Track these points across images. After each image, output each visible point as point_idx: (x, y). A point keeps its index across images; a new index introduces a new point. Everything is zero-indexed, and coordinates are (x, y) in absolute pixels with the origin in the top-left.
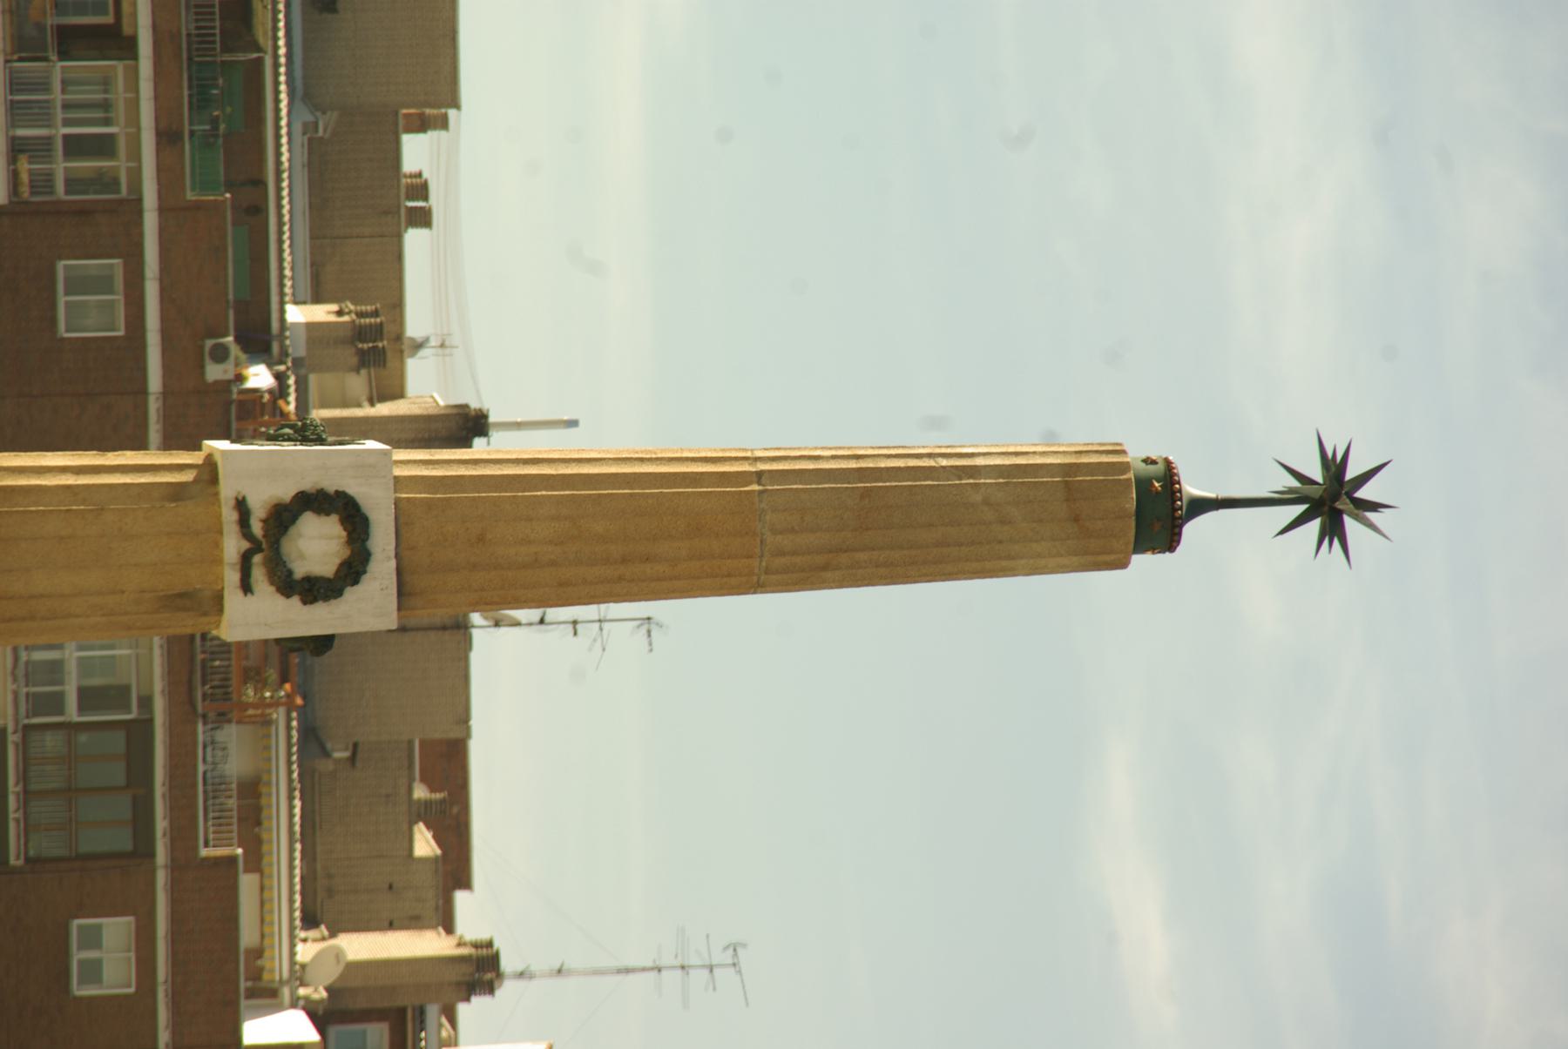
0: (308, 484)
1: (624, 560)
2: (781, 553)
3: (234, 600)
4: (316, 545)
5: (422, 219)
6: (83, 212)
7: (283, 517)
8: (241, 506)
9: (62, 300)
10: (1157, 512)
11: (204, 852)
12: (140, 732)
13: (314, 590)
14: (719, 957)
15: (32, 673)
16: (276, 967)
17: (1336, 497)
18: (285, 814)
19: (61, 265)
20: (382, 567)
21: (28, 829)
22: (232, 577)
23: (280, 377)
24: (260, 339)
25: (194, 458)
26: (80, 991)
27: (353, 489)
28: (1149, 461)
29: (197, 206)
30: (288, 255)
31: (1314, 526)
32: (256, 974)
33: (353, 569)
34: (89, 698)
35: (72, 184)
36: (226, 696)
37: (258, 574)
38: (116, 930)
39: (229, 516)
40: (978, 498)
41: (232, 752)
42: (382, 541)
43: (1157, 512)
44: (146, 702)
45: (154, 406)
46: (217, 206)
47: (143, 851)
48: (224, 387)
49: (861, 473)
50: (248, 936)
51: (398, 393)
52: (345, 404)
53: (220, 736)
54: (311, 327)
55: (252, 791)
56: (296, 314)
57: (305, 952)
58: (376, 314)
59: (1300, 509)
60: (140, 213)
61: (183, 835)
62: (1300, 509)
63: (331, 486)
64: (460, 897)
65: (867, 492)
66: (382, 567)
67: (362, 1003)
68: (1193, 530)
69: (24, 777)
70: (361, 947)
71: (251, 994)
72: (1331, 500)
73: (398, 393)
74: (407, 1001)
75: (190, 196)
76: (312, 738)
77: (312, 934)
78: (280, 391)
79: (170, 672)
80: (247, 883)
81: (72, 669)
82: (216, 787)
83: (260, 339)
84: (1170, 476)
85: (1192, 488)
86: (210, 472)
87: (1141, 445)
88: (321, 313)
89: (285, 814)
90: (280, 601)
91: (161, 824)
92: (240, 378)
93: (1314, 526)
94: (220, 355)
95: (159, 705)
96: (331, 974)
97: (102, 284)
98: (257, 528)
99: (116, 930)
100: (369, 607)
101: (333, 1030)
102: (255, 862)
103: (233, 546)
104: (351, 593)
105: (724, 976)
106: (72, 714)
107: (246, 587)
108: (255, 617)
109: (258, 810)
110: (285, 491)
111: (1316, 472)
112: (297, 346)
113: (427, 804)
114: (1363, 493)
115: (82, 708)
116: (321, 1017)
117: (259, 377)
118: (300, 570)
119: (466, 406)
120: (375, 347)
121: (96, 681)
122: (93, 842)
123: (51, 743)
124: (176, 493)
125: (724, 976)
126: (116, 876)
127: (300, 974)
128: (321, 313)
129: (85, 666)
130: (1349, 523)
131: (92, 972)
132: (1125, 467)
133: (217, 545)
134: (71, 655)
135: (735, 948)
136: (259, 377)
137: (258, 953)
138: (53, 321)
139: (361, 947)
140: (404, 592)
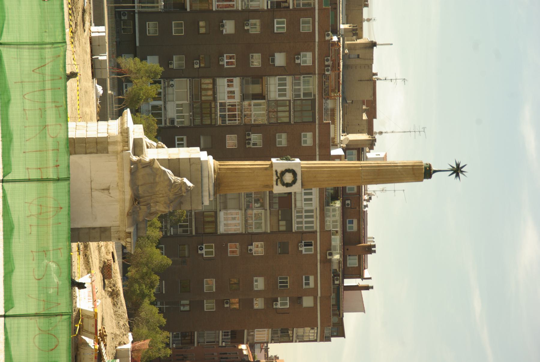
0: (287, 168)
1: (339, 180)
2: (365, 179)
3: (275, 187)
4: (288, 178)
5: (367, 6)
6: (306, 10)
7: (283, 173)
8: (276, 171)
9: (301, 25)
10: (428, 172)
11: (324, 122)
12: (314, 101)
13: (288, 185)
14: (421, 130)
15: (295, 90)
16: (337, 141)
17: (458, 170)
18: (340, 114)
19: (301, 19)
20: (299, 182)
21: (294, 117)
22: (275, 183)
23: (339, 39)
24: (335, 31)
25: (269, 163)
26: (303, 145)
27: (294, 169)
28: (427, 164)
29: (325, 9)
30: (341, 17)
31: (455, 175)
32: (334, 142)
33: (294, 182)
34: (305, 94)
35: (304, 5)
36: (328, 95)
37: (279, 183)
38: (309, 135)
39: (274, 173)
40: (398, 170)
41: (330, 104)
42: (299, 177)
43: (428, 172)
44: (315, 95)
45: (317, 44)
46: (328, 9)
47: (314, 121)
48: (329, 41)
49: (378, 166)
50: (332, 135)
51: (361, 37)
52: (352, 41)
53: (327, 102)
54: (345, 29)
55: (333, 111)
56: (342, 26)
57: (342, 138)
58: (356, 26)
59: (452, 172)
60: (315, 10)
61: (321, 119)
62: (452, 172)
63: (291, 168)
64: (374, 120)
65: (379, 170)
66: (299, 182)
67: (352, 147)
68: (434, 176)
69: (294, 108)
70: (352, 137)
71: (333, 145)
72: (457, 171)
73: (361, 37)
74: (360, 147)
75: (324, 7)
76: (344, 100)
77: (344, 134)
78: (339, 41)
79: (319, 91)
80: (332, 126)
81: (302, 89)
82: (326, 110)
83: (335, 31)
84: (430, 167)
85: (434, 168)
86: (271, 165)
87: (425, 161)
88: (347, 26)
89: (340, 114)
90: (282, 187)
91: (317, 117)
92: (332, 39)
93: (455, 175)
94: (328, 35)
95: (317, 96)
96: (347, 142)
97: (308, 22)
98: (279, 175)
99: (309, 135)
100: (296, 188)
101: (347, 151)
102: (333, 122)
103: (275, 178)
104: (294, 186)
105: (422, 133)
106: (302, 97)
107: (277, 184)
108: (279, 189)
109: (334, 114)
110: (283, 169)
111: (455, 167)
112: (342, 32)
113: (366, 109)
114: (462, 170)
115: (304, 96)
116: (344, 150)
117: (335, 39)
118: (286, 182)
119: (372, 41)
120: (356, 32)
121: (306, 92)
122: (305, 120)
123: (299, 102)
124: (266, 169)
125: (422, 133)
126: (309, 125)
127: (341, 142)
128: (347, 26)
129: (304, 89)
130: (460, 174)
131: (305, 142)
132: (422, 165)
133: (273, 178)
134: (302, 87)
135: (424, 128)
136: (335, 39)
137: (334, 138)
138: (300, 29)
139: (352, 137)
140: (303, 185)
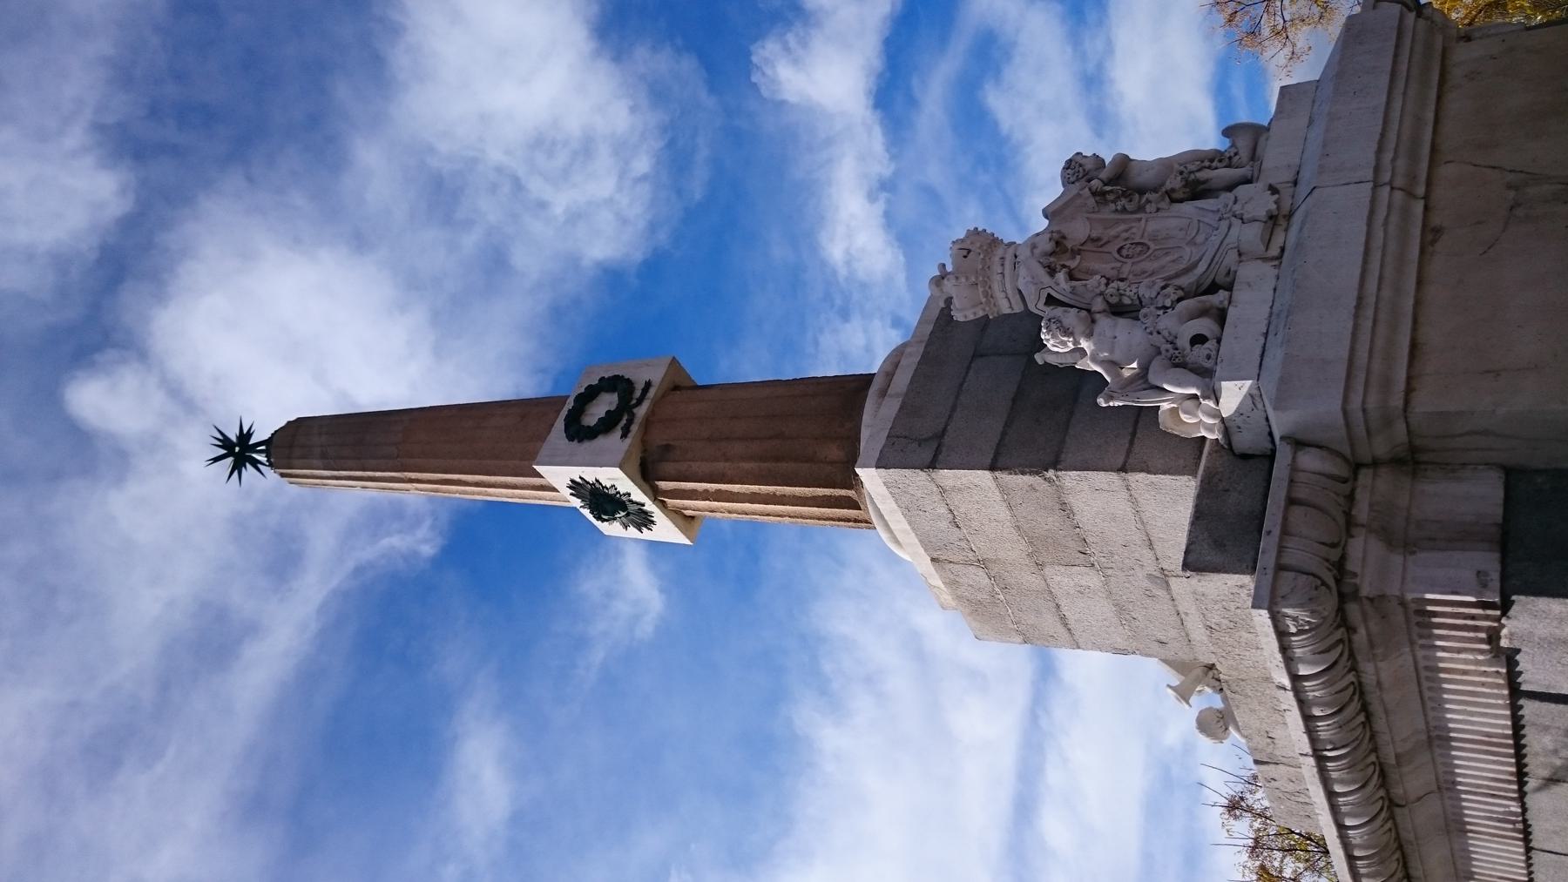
0: (587, 445)
7: (607, 425)
8: (624, 436)
22: (652, 392)
37: (638, 394)
39: (634, 428)
103: (641, 411)
107: (648, 385)
110: (601, 441)
